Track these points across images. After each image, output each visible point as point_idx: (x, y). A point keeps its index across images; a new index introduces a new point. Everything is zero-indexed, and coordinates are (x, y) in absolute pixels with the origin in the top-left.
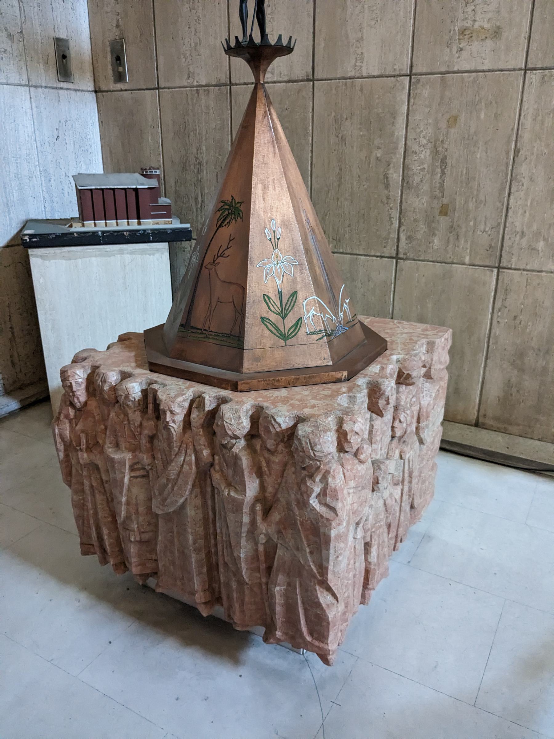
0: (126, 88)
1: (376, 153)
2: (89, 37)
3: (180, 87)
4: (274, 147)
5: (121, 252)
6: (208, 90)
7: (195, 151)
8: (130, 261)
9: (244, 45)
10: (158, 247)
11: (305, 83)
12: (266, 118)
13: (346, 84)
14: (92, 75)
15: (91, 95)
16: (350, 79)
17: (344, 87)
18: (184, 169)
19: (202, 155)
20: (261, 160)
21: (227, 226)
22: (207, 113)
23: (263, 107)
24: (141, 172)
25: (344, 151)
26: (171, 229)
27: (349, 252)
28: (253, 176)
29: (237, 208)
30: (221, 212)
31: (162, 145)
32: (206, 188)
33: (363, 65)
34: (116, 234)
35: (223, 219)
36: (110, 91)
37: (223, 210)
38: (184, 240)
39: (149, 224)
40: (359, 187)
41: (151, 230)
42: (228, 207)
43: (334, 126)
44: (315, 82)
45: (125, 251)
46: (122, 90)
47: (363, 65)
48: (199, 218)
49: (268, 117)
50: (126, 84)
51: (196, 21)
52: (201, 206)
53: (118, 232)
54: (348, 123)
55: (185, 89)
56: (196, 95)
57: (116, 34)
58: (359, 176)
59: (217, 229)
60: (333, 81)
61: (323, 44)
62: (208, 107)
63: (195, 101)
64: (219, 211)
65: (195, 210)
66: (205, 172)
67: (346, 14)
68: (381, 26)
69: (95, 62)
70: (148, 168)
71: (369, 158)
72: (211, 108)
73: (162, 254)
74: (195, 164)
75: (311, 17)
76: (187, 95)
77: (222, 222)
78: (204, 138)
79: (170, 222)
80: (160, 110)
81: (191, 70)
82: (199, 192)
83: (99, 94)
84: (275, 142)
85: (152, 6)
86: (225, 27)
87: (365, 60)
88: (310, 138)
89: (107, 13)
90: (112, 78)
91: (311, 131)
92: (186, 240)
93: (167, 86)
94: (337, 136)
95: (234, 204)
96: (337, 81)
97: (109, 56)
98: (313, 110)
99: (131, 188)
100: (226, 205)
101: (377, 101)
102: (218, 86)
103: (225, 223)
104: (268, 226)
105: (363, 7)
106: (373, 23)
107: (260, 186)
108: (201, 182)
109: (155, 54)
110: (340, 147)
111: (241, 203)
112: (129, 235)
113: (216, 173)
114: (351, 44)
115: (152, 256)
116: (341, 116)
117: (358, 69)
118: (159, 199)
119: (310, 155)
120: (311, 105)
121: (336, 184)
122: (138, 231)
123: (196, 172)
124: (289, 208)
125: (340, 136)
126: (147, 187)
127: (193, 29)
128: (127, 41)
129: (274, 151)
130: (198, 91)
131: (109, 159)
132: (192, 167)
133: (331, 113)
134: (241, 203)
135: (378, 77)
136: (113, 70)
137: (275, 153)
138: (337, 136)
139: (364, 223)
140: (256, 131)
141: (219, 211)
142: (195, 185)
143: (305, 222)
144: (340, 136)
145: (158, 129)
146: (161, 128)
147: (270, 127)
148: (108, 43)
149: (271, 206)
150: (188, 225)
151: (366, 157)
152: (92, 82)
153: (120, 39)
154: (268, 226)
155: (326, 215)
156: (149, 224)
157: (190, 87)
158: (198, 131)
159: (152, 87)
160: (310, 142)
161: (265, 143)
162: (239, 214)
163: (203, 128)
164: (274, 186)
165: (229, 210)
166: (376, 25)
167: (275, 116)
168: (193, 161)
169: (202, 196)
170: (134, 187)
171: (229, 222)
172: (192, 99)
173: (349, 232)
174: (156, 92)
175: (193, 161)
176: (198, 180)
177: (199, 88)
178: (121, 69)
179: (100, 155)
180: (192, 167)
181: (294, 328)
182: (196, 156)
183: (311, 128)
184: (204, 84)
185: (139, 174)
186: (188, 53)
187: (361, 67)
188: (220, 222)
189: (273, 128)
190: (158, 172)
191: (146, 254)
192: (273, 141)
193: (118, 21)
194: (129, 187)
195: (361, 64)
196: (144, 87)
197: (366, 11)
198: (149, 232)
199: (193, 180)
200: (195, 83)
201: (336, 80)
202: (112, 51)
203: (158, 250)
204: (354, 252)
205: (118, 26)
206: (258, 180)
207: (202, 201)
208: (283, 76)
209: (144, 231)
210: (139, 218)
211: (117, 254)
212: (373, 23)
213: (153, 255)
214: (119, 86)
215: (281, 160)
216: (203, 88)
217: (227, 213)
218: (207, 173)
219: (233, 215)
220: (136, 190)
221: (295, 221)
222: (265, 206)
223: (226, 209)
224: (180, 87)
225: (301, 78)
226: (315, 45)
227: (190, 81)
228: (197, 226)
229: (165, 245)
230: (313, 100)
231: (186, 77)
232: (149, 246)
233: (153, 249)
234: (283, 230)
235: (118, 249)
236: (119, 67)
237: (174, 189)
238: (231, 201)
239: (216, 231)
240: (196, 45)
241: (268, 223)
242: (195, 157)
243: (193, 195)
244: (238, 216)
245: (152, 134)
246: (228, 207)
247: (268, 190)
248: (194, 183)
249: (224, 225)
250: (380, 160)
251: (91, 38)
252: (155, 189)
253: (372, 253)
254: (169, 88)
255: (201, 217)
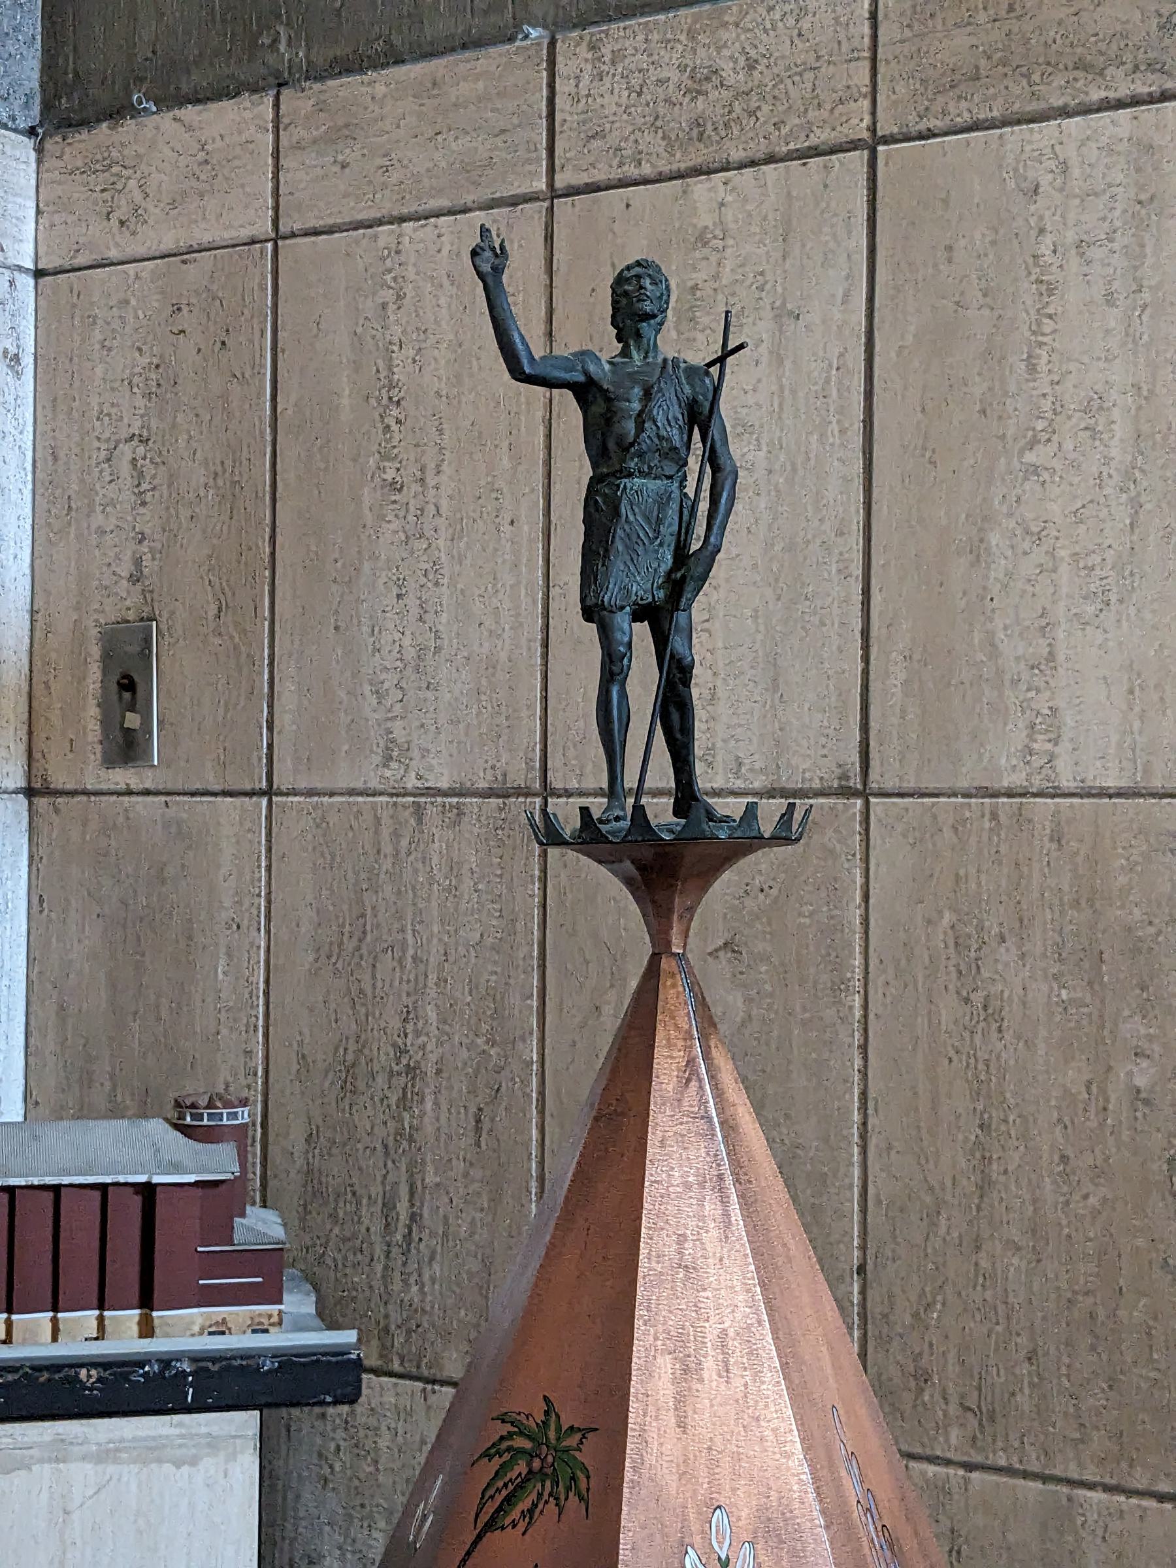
0: (148, 785)
1: (1130, 1074)
2: (28, 607)
3: (352, 792)
4: (724, 1200)
5: (59, 1454)
6: (458, 806)
7: (395, 1023)
8: (90, 1492)
9: (612, 833)
10: (215, 1430)
11: (832, 801)
12: (694, 1084)
13: (994, 816)
14: (23, 733)
15: (9, 804)
16: (1010, 795)
17: (987, 825)
18: (348, 1088)
19: (424, 1039)
20: (671, 1250)
21: (521, 1526)
22: (452, 890)
23: (680, 1043)
24: (172, 1114)
25: (998, 1057)
26: (276, 1354)
27: (1035, 1467)
28: (638, 1323)
29: (567, 1450)
30: (497, 1462)
31: (267, 993)
32: (430, 1169)
33: (1057, 750)
34: (45, 1376)
35: (504, 1493)
36: (85, 792)
37: (506, 1457)
38: (329, 1399)
39: (185, 1330)
40: (1067, 1203)
41: (196, 1358)
42: (527, 1445)
43: (953, 962)
44: (872, 800)
45: (76, 1449)
46: (129, 793)
47: (1057, 750)
48: (397, 1285)
49: (700, 1080)
50: (149, 773)
51: (425, 575)
52: (408, 1236)
53: (54, 1366)
54: (1007, 954)
55: (370, 799)
56: (413, 822)
57: (128, 603)
58: (1064, 1159)
59: (479, 1537)
60: (942, 800)
61: (899, 674)
62: (453, 867)
63: (404, 843)
64: (487, 1455)
65: (379, 1251)
66: (429, 1105)
67: (987, 577)
68: (1125, 624)
69: (39, 689)
70: (203, 1101)
71: (1103, 1091)
72: (465, 871)
73: (232, 1457)
74: (391, 1071)
75: (852, 580)
76: (378, 820)
77: (500, 1509)
78: (432, 978)
79: (275, 1319)
80: (269, 869)
81: (399, 734)
82: (404, 1177)
83: (42, 802)
84: (729, 1180)
85: (268, 520)
86: (535, 602)
87: (1067, 734)
88: (857, 1001)
89: (101, 532)
90: (99, 748)
91: (858, 974)
92: (336, 1403)
93: (302, 785)
94: (967, 1000)
95: (552, 1435)
96: (960, 800)
97: (95, 673)
98: (866, 897)
99: (126, 1184)
100: (521, 1433)
101: (1123, 880)
102: (498, 796)
103: (515, 1514)
104: (697, 1540)
105: (1051, 553)
106: (1090, 609)
107: (665, 1366)
108: (411, 1140)
109: (266, 677)
110: (978, 1038)
111: (585, 1432)
112: (99, 1380)
113: (473, 1110)
114: (1007, 677)
115: (185, 1469)
116: (980, 928)
117: (1042, 762)
118: (237, 1220)
119: (858, 1063)
120: (859, 880)
121: (968, 1185)
122: (138, 1362)
123: (394, 1099)
124: (787, 1455)
125: (978, 998)
126: (191, 1178)
127: (412, 601)
128: (164, 627)
129: (726, 1214)
130: (418, 810)
131: (51, 1035)
132: (381, 1080)
133: (940, 913)
134: (585, 1432)
135: (1120, 794)
136: (105, 723)
137: (728, 1224)
138: (967, 1000)
139: (1093, 1348)
140: (653, 1140)
141: (487, 1455)
142: (387, 1154)
143: (856, 1513)
144: (978, 998)
145: (256, 934)
146: (268, 932)
147: (710, 1120)
148: (94, 632)
149: (710, 1448)
150: (349, 1337)
151: (1089, 1085)
152: (22, 761)
153: (142, 620)
154: (697, 1540)
155: (929, 1307)
156: (185, 1330)
157: (392, 795)
158: (411, 952)
159: (248, 787)
160: (858, 1013)
161: (688, 1186)
162: (573, 1478)
163: (429, 941)
164: (726, 1363)
165: (531, 1456)
166: (1102, 616)
167: (728, 1077)
168: (384, 1056)
169: (412, 1193)
170: (142, 1179)
171: (531, 1511)
172: (396, 835)
173: (1032, 1385)
174: (259, 805)
175: (384, 1056)
176: (399, 1133)
177: (423, 800)
178: (132, 720)
179: (21, 1018)
180: (381, 1080)
181: (708, 469)
182: (400, 1041)
183: (858, 961)
184: (444, 784)
185: (167, 1120)
186: (390, 680)
187: (1052, 758)
188: (490, 1508)
189: (721, 1124)
190: (243, 1116)
191: (160, 1461)
192: (721, 1177)
193: (138, 562)
194: (121, 1179)
195: (1049, 746)
196: (217, 788)
197: (1064, 569)
198: (186, 1367)
199: (380, 1131)
200: (411, 782)
201: (955, 795)
202: (107, 658)
203: (213, 1443)
204: (1058, 1472)
205: (135, 579)
206: (656, 1339)
207: (413, 1217)
208: (749, 775)
209: (166, 1361)
210: (146, 1301)
211: (41, 1461)
212: (1090, 609)
213: (193, 1462)
214: (121, 777)
215: (756, 1253)
216: (439, 799)
217: (521, 1467)
218: (436, 1104)
219: (548, 1484)
220: (147, 1190)
221: (816, 1514)
222: (685, 1448)
223: (521, 1451)
224: (352, 792)
225: (816, 784)
226: (872, 676)
227: (393, 772)
228: (387, 1316)
229: (247, 1422)
230: (866, 860)
231: (377, 759)
232: (180, 1425)
233: (192, 1436)
234: (762, 1558)
235: (47, 1438)
236: (128, 714)
237: (300, 1162)
238: (540, 1418)
239: (475, 1543)
240: (421, 650)
241: (695, 1527)
242: (394, 1045)
243: (376, 1190)
244: (568, 1489)
245: (229, 955)
246: (527, 1445)
247: (701, 1380)
248: (386, 1147)
249: (507, 1521)
250: (1147, 1102)
251: (33, 612)
252: (223, 1187)
253: (1140, 1481)
254: (311, 793)
255: (405, 1282)
